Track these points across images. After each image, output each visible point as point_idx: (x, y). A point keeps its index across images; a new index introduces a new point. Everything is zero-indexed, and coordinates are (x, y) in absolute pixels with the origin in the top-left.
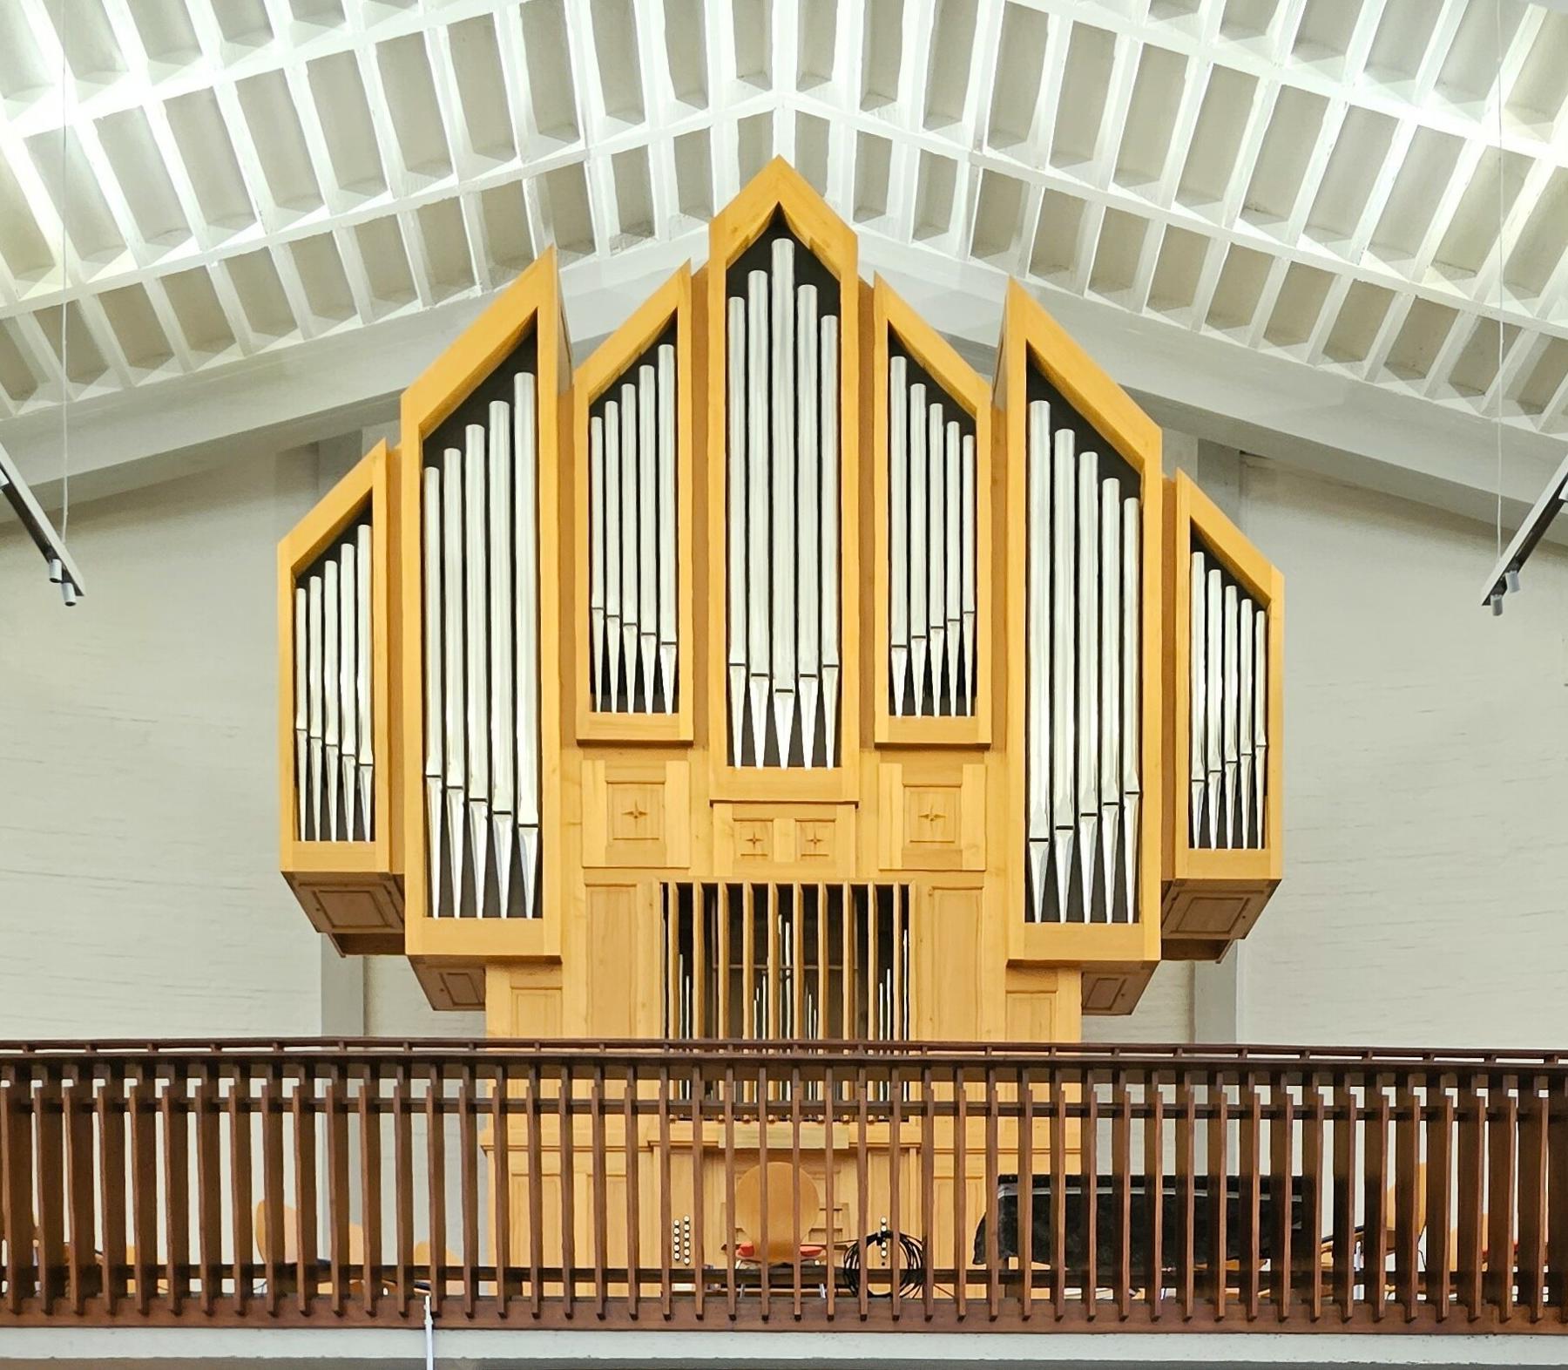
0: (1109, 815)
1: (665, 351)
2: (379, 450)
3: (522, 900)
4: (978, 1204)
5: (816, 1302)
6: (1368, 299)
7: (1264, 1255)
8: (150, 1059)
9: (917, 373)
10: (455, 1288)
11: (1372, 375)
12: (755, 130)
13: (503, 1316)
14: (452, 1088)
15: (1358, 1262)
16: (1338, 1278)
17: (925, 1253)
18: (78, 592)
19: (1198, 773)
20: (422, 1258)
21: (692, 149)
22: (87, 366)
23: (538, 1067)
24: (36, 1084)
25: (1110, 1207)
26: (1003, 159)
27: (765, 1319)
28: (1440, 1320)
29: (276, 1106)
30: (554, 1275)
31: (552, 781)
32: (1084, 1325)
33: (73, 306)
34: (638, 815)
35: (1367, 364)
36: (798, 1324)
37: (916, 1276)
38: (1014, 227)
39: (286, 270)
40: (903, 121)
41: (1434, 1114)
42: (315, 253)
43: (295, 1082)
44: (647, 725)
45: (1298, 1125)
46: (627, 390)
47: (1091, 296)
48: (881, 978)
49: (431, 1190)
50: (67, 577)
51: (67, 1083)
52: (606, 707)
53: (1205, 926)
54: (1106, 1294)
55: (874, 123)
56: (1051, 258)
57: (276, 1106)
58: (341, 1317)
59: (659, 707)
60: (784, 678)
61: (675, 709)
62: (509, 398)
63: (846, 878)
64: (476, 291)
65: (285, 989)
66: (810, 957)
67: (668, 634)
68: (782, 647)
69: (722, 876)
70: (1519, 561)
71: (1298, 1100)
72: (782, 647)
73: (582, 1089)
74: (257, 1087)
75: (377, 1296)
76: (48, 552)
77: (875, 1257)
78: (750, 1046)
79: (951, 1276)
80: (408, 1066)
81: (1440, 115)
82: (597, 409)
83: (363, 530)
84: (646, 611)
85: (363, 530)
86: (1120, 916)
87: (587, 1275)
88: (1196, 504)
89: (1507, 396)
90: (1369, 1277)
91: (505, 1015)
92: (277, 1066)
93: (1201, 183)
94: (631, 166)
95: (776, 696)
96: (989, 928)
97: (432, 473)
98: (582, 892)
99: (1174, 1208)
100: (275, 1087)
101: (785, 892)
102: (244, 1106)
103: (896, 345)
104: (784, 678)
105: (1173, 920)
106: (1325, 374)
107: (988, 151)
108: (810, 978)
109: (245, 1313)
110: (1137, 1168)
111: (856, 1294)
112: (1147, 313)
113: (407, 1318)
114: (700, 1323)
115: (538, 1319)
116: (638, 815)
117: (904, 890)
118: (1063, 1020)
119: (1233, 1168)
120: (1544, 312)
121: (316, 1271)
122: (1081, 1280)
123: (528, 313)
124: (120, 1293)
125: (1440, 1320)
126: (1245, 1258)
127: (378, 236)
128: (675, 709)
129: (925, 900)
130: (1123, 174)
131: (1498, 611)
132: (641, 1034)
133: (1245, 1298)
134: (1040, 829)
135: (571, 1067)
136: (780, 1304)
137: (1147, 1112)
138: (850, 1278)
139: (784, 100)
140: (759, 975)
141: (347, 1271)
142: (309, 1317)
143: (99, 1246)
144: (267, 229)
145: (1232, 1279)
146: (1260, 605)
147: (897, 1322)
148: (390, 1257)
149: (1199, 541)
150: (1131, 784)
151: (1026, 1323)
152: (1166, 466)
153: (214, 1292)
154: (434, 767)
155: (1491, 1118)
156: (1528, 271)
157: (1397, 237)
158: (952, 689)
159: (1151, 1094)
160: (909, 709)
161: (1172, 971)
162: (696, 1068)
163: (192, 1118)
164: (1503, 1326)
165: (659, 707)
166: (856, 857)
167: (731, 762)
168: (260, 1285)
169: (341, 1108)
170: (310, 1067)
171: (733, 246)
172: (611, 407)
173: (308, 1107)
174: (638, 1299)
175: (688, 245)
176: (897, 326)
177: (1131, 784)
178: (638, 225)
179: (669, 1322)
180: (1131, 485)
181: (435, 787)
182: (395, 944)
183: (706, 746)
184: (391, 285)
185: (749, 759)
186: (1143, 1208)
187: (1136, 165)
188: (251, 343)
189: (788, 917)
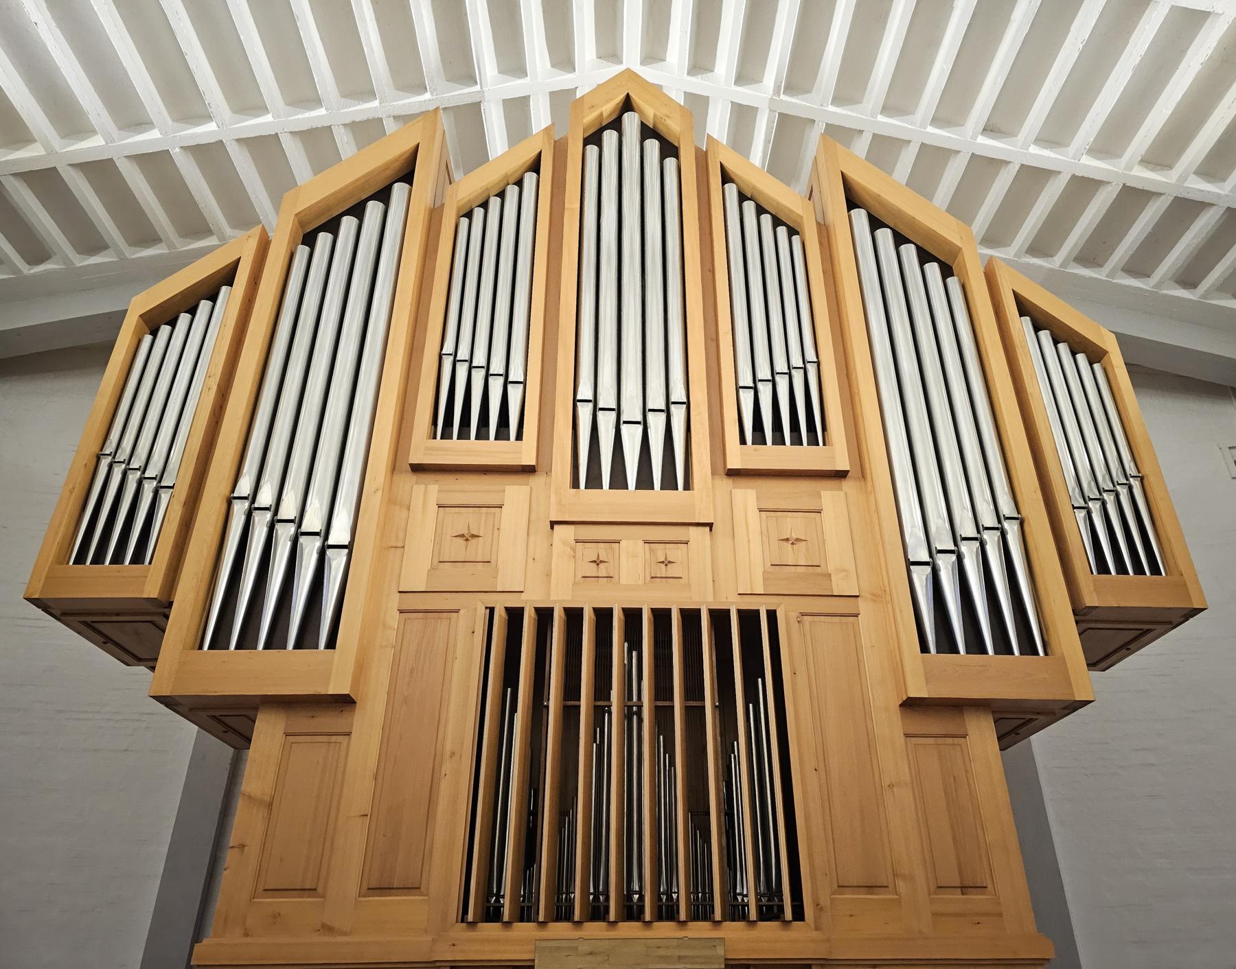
26: (796, 104)
44: (491, 451)
60: (632, 411)
61: (519, 436)
63: (704, 600)
67: (516, 374)
69: (560, 597)
95: (624, 428)
98: (394, 619)
101: (633, 616)
104: (632, 411)
106: (1028, 264)
108: (663, 717)
117: (772, 615)
123: (412, 145)
128: (519, 436)
140: (600, 713)
149: (1024, 307)
156: (1213, 167)
167: (575, 484)
176: (725, 164)
183: (548, 472)
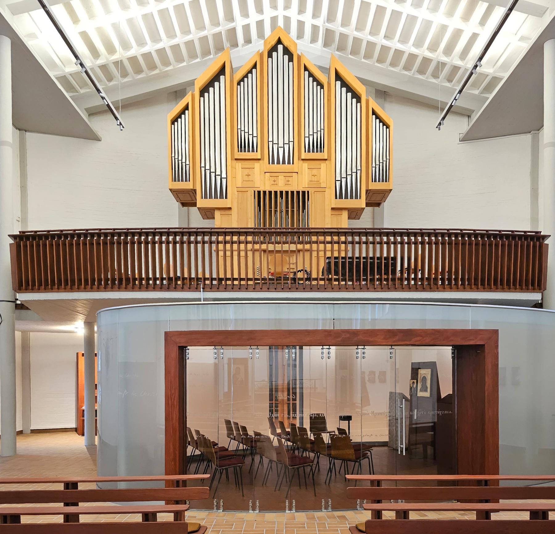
0: (354, 175)
1: (254, 70)
2: (190, 93)
3: (223, 195)
4: (322, 264)
5: (287, 285)
6: (412, 57)
7: (377, 275)
8: (141, 232)
9: (311, 75)
10: (207, 282)
11: (413, 74)
12: (274, 20)
13: (218, 288)
14: (207, 238)
15: (406, 275)
16: (401, 279)
17: (311, 274)
18: (123, 127)
19: (374, 165)
20: (200, 276)
21: (260, 24)
22: (124, 74)
23: (225, 234)
24: (115, 238)
25: (351, 264)
26: (330, 26)
27: (275, 289)
28: (424, 288)
29: (168, 243)
30: (229, 279)
31: (229, 168)
32: (345, 290)
33: (121, 61)
34: (248, 175)
35: (413, 71)
36: (283, 290)
37: (309, 279)
38: (333, 41)
39: (169, 52)
40: (308, 18)
41: (422, 243)
42: (175, 48)
43: (172, 237)
44: (250, 155)
45: (413, 246)
46: (246, 79)
47: (350, 56)
48: (303, 212)
49: (203, 261)
50: (121, 124)
51: (122, 238)
52: (241, 151)
53: (376, 199)
54: (351, 283)
55: (301, 18)
56: (341, 48)
57: (168, 243)
58: (183, 289)
59: (253, 151)
60: (281, 144)
61: (257, 151)
62: (214, 87)
63: (295, 189)
64: (212, 56)
65: (169, 216)
66: (287, 207)
67: (255, 135)
68: (281, 137)
69: (267, 189)
70: (444, 118)
71: (406, 241)
72: (281, 137)
73: (235, 238)
74: (164, 238)
75: (190, 284)
76: (116, 118)
77: (300, 275)
78: (274, 229)
79: (316, 279)
80: (197, 234)
81: (429, 16)
82: (239, 84)
83: (187, 112)
84: (250, 128)
85: (187, 112)
86: (356, 198)
87: (236, 279)
88: (373, 104)
89: (444, 79)
90: (408, 279)
91: (219, 221)
92: (168, 234)
93: (374, 31)
94: (246, 28)
96: (327, 202)
97: (202, 99)
98: (236, 193)
99: (365, 264)
100: (168, 238)
101: (281, 192)
102: (161, 243)
103: (306, 69)
104: (281, 144)
105: (368, 199)
107: (327, 24)
108: (287, 212)
109: (162, 288)
110: (357, 255)
111: (295, 283)
112: (363, 60)
113: (197, 289)
114: (261, 290)
115: (226, 289)
116: (248, 175)
117: (308, 192)
118: (344, 222)
119: (385, 255)
120: (452, 60)
121: (177, 279)
122: (344, 280)
124: (134, 284)
125: (424, 288)
126: (381, 275)
127: (190, 44)
128: (257, 151)
129: (313, 194)
130: (357, 29)
131: (439, 129)
132: (249, 226)
133: (381, 284)
134: (338, 178)
135: (232, 234)
136: (279, 285)
137: (373, 243)
138: (294, 279)
139: (281, 13)
140: (276, 211)
141: (184, 279)
142: (176, 289)
143: (129, 273)
144: (165, 43)
145: (378, 280)
146: (388, 127)
147: (304, 290)
148: (193, 276)
149: (374, 113)
150: (359, 168)
151: (333, 290)
152: (366, 96)
153: (155, 284)
154: (203, 165)
155: (442, 244)
157: (419, 43)
158: (319, 147)
159: (360, 239)
160: (309, 151)
161: (369, 210)
162: (262, 233)
163: (157, 245)
164: (437, 290)
165: (253, 151)
166: (297, 185)
167: (269, 163)
168: (165, 282)
169: (182, 243)
170: (175, 234)
171: (269, 46)
172: (242, 83)
173: (175, 243)
174: (248, 285)
175: (259, 46)
177: (359, 168)
178: (248, 41)
179: (254, 290)
180: (359, 100)
181: (203, 169)
182: (194, 205)
183: (263, 160)
184: (193, 55)
185: (273, 163)
186: (358, 264)
187: (360, 27)
188: (161, 68)
189: (282, 198)
